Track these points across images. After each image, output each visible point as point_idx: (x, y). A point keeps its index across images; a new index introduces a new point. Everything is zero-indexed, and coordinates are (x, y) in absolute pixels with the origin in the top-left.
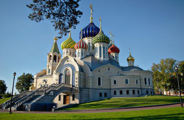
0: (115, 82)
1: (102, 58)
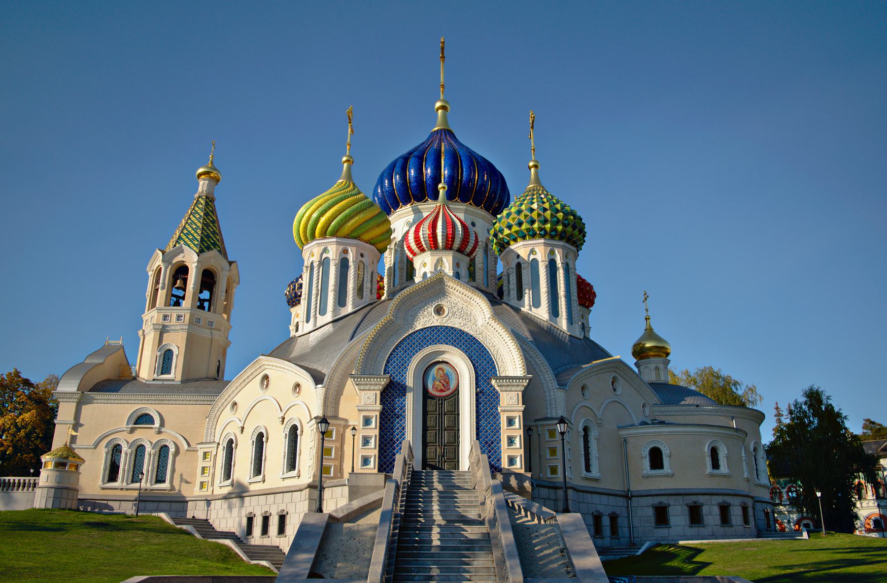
0: (656, 458)
1: (563, 323)
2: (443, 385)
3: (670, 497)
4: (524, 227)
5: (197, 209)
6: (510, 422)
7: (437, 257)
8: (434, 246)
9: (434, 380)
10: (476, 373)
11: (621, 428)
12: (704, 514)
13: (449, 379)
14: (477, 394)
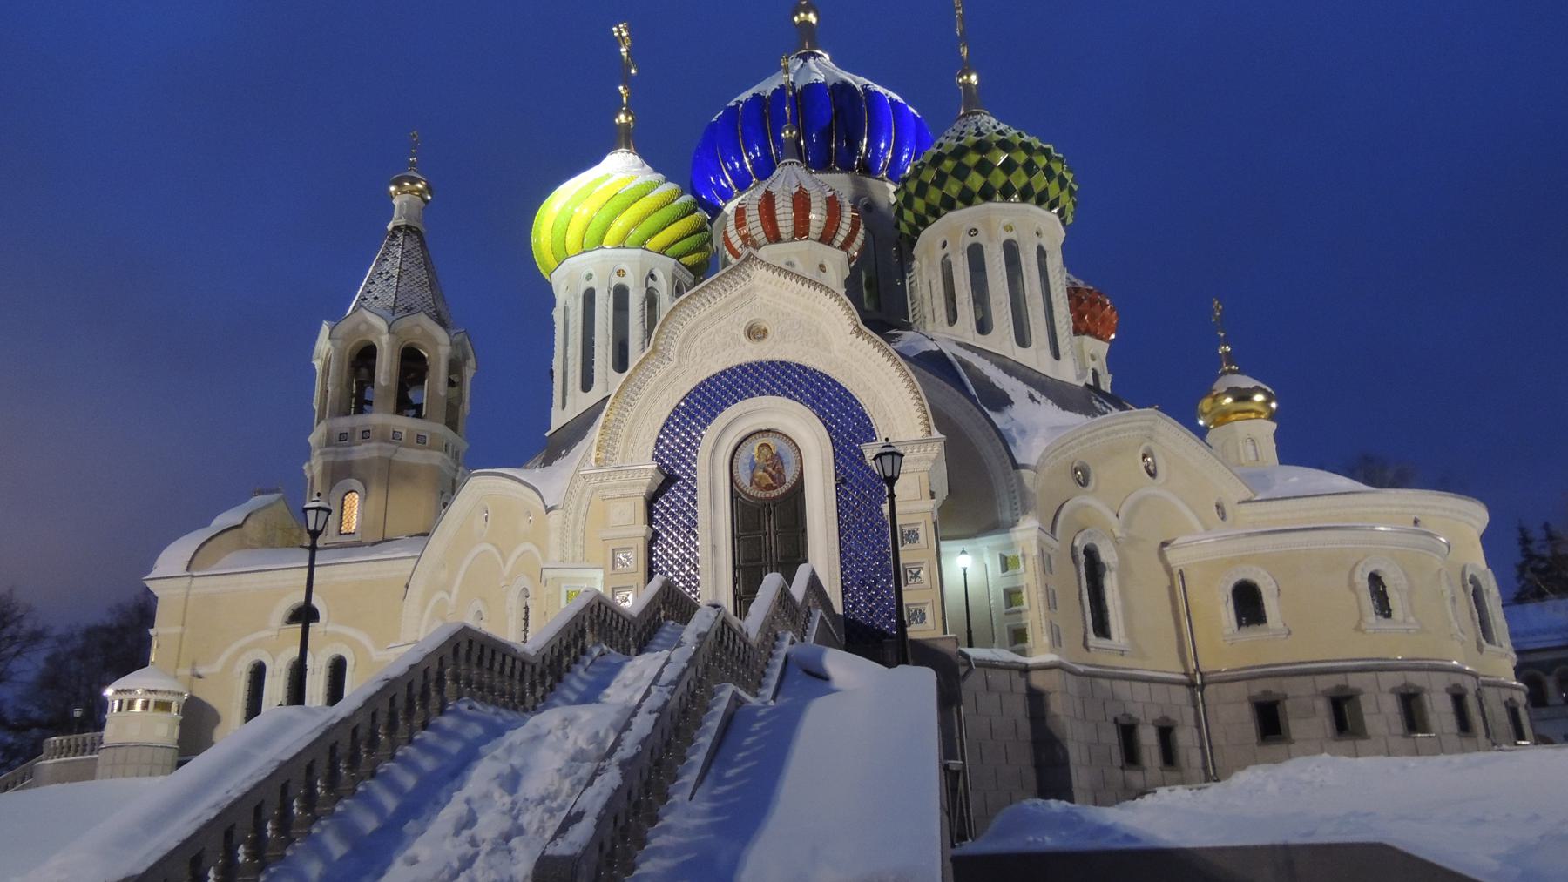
0: (1248, 602)
2: (771, 475)
13: (782, 464)
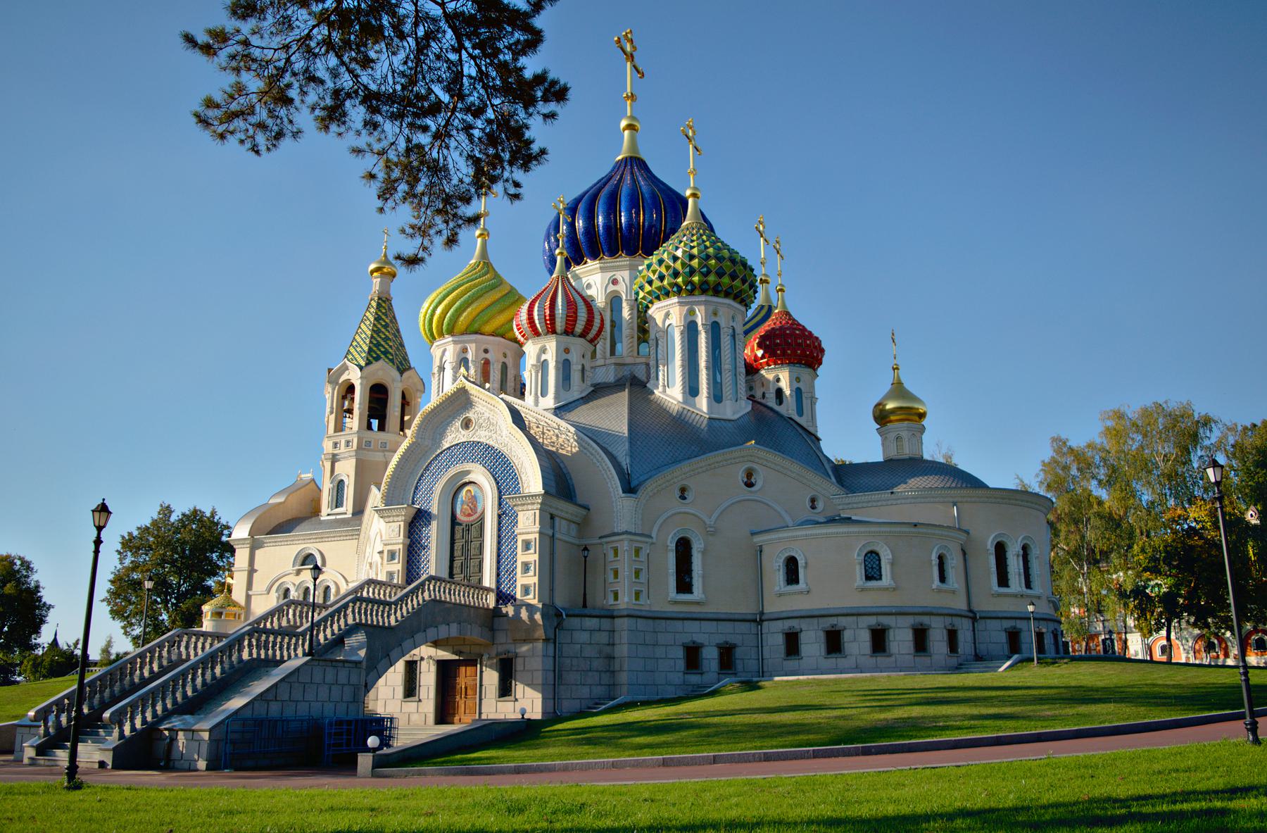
0: (792, 570)
3: (802, 620)
4: (665, 282)
5: (368, 314)
6: (527, 545)
7: (539, 346)
8: (537, 334)
9: (463, 503)
10: (498, 489)
11: (753, 534)
12: (845, 640)
14: (499, 516)
